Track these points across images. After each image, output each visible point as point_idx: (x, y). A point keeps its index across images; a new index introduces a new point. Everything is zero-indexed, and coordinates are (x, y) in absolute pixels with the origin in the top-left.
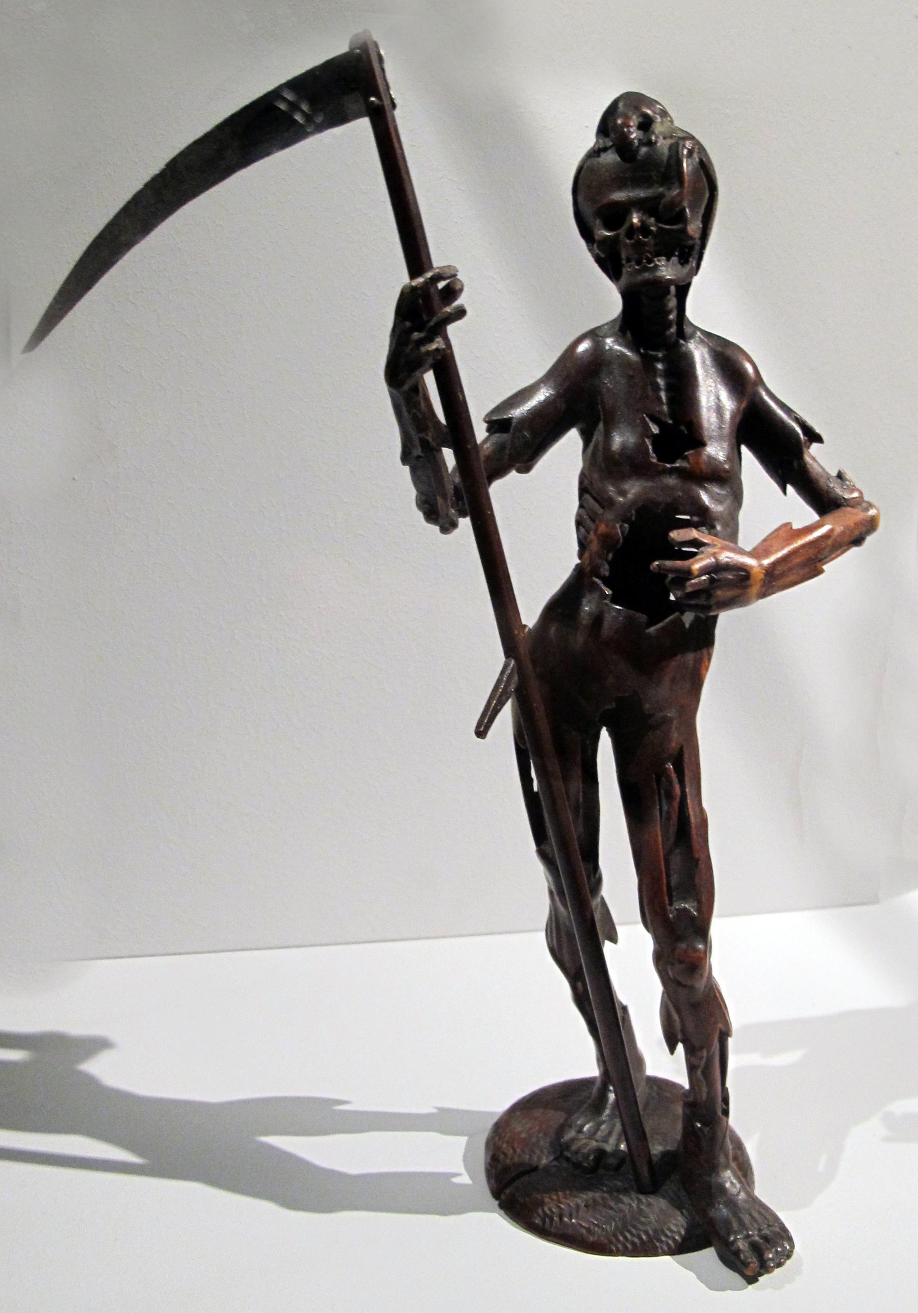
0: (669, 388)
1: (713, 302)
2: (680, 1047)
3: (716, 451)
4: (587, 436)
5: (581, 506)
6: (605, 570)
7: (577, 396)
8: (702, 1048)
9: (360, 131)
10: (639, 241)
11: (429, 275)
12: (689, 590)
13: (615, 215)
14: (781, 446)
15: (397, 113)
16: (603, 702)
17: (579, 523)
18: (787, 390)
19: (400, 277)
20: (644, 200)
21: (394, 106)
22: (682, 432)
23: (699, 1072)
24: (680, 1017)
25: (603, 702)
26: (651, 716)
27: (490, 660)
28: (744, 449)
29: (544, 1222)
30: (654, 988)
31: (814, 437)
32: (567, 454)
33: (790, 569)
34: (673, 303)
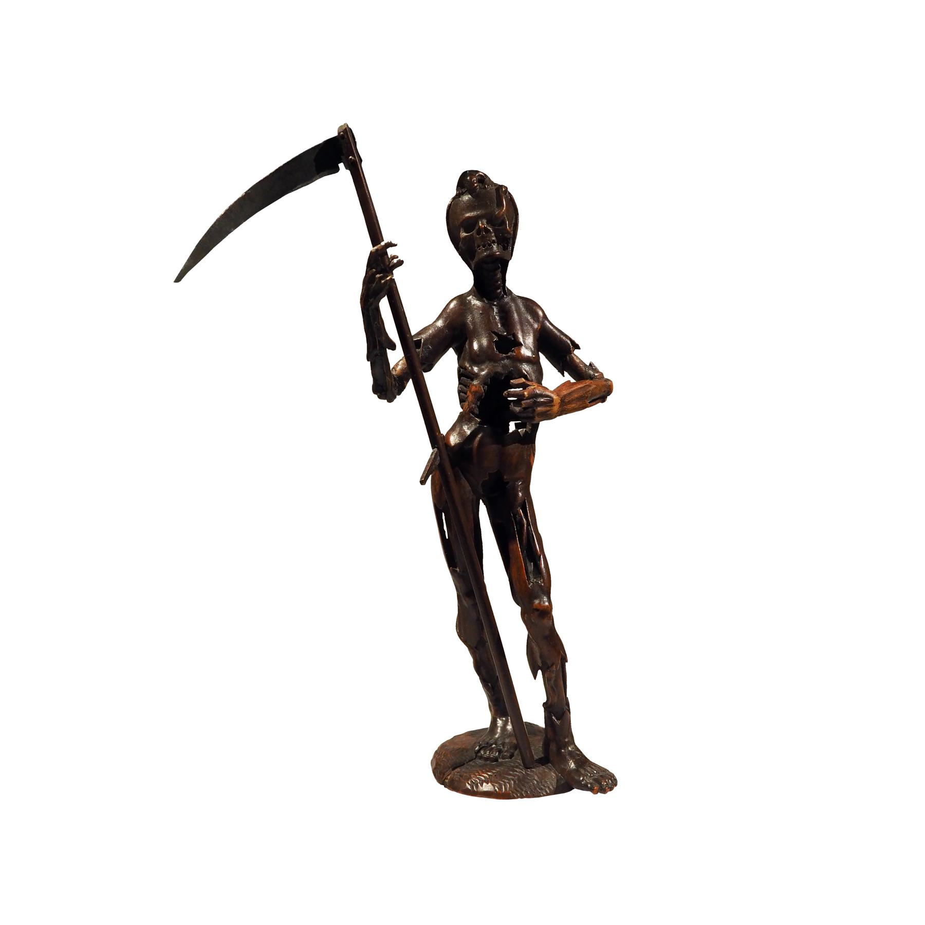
0: (501, 318)
1: (519, 279)
2: (540, 672)
3: (526, 352)
4: (459, 352)
5: (460, 383)
6: (477, 411)
7: (453, 332)
8: (552, 665)
9: (344, 174)
10: (483, 236)
11: (383, 244)
12: (524, 406)
13: (470, 225)
14: (558, 348)
15: (363, 164)
16: (482, 486)
17: (459, 392)
18: (561, 319)
19: (366, 247)
20: (483, 220)
21: (361, 161)
22: (508, 344)
23: (552, 682)
24: (539, 648)
25: (482, 486)
26: (508, 483)
27: (424, 451)
28: (541, 355)
29: (472, 787)
30: (522, 633)
31: (577, 347)
32: (449, 361)
33: (573, 400)
34: (499, 275)
